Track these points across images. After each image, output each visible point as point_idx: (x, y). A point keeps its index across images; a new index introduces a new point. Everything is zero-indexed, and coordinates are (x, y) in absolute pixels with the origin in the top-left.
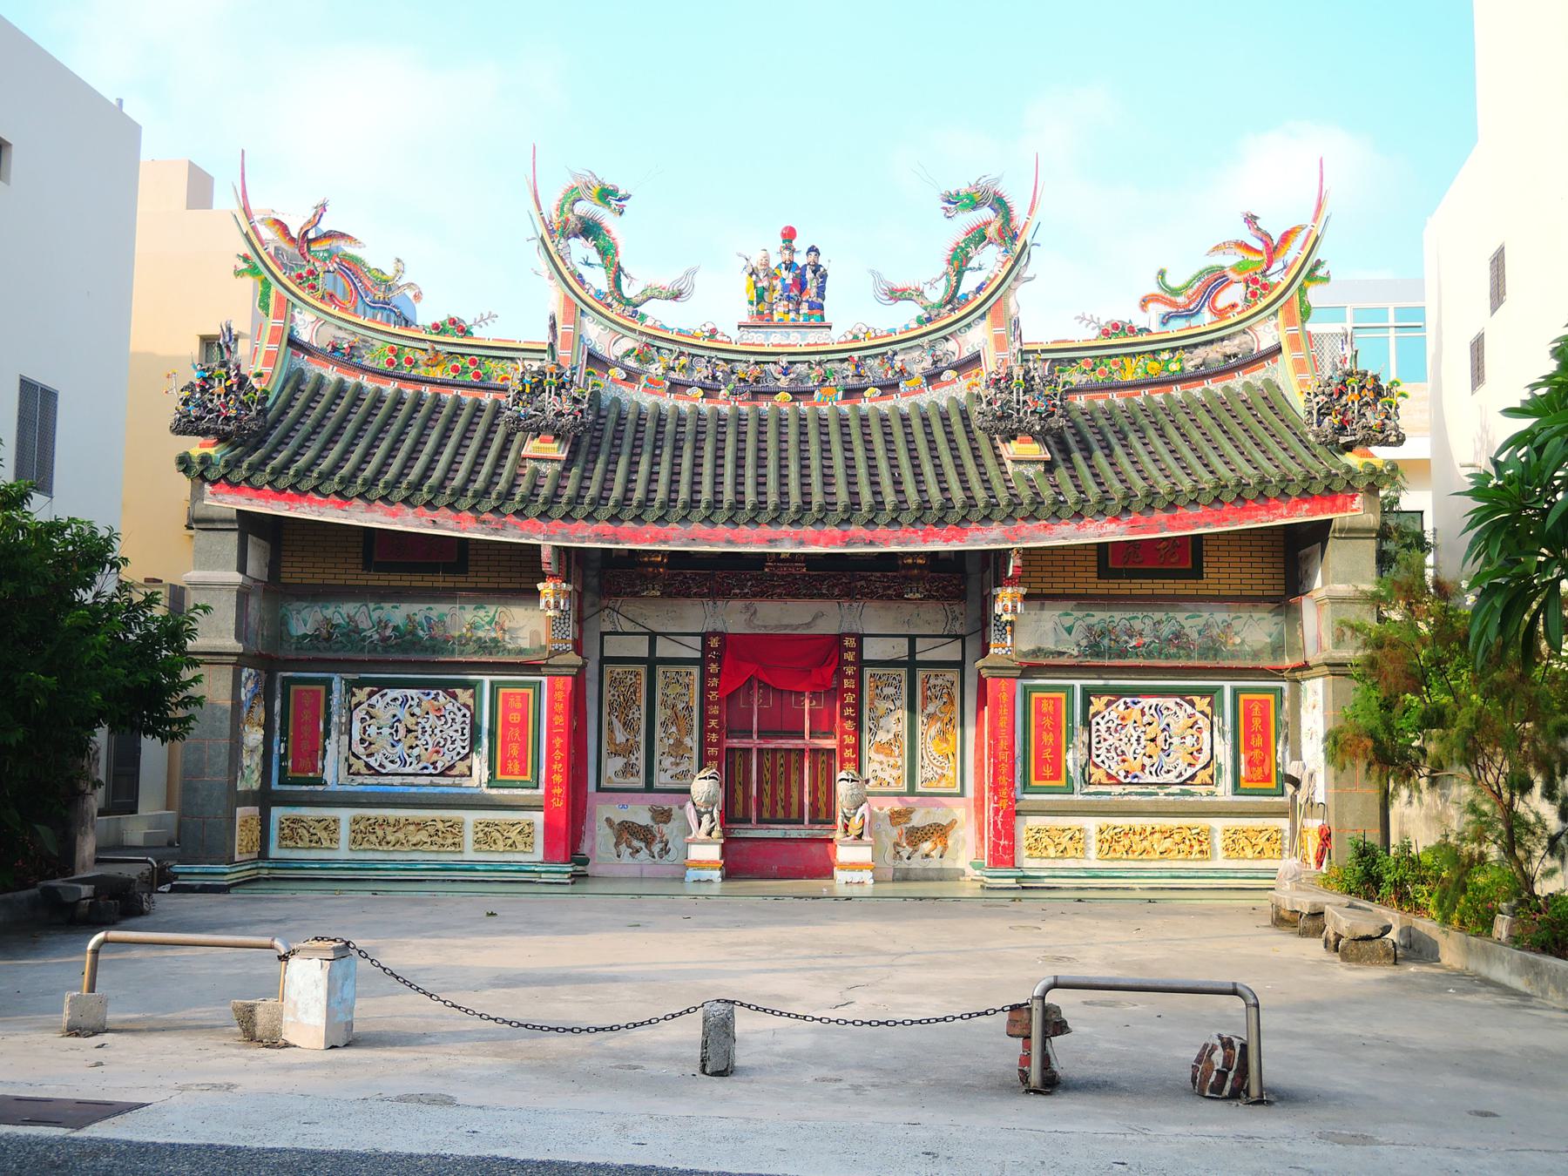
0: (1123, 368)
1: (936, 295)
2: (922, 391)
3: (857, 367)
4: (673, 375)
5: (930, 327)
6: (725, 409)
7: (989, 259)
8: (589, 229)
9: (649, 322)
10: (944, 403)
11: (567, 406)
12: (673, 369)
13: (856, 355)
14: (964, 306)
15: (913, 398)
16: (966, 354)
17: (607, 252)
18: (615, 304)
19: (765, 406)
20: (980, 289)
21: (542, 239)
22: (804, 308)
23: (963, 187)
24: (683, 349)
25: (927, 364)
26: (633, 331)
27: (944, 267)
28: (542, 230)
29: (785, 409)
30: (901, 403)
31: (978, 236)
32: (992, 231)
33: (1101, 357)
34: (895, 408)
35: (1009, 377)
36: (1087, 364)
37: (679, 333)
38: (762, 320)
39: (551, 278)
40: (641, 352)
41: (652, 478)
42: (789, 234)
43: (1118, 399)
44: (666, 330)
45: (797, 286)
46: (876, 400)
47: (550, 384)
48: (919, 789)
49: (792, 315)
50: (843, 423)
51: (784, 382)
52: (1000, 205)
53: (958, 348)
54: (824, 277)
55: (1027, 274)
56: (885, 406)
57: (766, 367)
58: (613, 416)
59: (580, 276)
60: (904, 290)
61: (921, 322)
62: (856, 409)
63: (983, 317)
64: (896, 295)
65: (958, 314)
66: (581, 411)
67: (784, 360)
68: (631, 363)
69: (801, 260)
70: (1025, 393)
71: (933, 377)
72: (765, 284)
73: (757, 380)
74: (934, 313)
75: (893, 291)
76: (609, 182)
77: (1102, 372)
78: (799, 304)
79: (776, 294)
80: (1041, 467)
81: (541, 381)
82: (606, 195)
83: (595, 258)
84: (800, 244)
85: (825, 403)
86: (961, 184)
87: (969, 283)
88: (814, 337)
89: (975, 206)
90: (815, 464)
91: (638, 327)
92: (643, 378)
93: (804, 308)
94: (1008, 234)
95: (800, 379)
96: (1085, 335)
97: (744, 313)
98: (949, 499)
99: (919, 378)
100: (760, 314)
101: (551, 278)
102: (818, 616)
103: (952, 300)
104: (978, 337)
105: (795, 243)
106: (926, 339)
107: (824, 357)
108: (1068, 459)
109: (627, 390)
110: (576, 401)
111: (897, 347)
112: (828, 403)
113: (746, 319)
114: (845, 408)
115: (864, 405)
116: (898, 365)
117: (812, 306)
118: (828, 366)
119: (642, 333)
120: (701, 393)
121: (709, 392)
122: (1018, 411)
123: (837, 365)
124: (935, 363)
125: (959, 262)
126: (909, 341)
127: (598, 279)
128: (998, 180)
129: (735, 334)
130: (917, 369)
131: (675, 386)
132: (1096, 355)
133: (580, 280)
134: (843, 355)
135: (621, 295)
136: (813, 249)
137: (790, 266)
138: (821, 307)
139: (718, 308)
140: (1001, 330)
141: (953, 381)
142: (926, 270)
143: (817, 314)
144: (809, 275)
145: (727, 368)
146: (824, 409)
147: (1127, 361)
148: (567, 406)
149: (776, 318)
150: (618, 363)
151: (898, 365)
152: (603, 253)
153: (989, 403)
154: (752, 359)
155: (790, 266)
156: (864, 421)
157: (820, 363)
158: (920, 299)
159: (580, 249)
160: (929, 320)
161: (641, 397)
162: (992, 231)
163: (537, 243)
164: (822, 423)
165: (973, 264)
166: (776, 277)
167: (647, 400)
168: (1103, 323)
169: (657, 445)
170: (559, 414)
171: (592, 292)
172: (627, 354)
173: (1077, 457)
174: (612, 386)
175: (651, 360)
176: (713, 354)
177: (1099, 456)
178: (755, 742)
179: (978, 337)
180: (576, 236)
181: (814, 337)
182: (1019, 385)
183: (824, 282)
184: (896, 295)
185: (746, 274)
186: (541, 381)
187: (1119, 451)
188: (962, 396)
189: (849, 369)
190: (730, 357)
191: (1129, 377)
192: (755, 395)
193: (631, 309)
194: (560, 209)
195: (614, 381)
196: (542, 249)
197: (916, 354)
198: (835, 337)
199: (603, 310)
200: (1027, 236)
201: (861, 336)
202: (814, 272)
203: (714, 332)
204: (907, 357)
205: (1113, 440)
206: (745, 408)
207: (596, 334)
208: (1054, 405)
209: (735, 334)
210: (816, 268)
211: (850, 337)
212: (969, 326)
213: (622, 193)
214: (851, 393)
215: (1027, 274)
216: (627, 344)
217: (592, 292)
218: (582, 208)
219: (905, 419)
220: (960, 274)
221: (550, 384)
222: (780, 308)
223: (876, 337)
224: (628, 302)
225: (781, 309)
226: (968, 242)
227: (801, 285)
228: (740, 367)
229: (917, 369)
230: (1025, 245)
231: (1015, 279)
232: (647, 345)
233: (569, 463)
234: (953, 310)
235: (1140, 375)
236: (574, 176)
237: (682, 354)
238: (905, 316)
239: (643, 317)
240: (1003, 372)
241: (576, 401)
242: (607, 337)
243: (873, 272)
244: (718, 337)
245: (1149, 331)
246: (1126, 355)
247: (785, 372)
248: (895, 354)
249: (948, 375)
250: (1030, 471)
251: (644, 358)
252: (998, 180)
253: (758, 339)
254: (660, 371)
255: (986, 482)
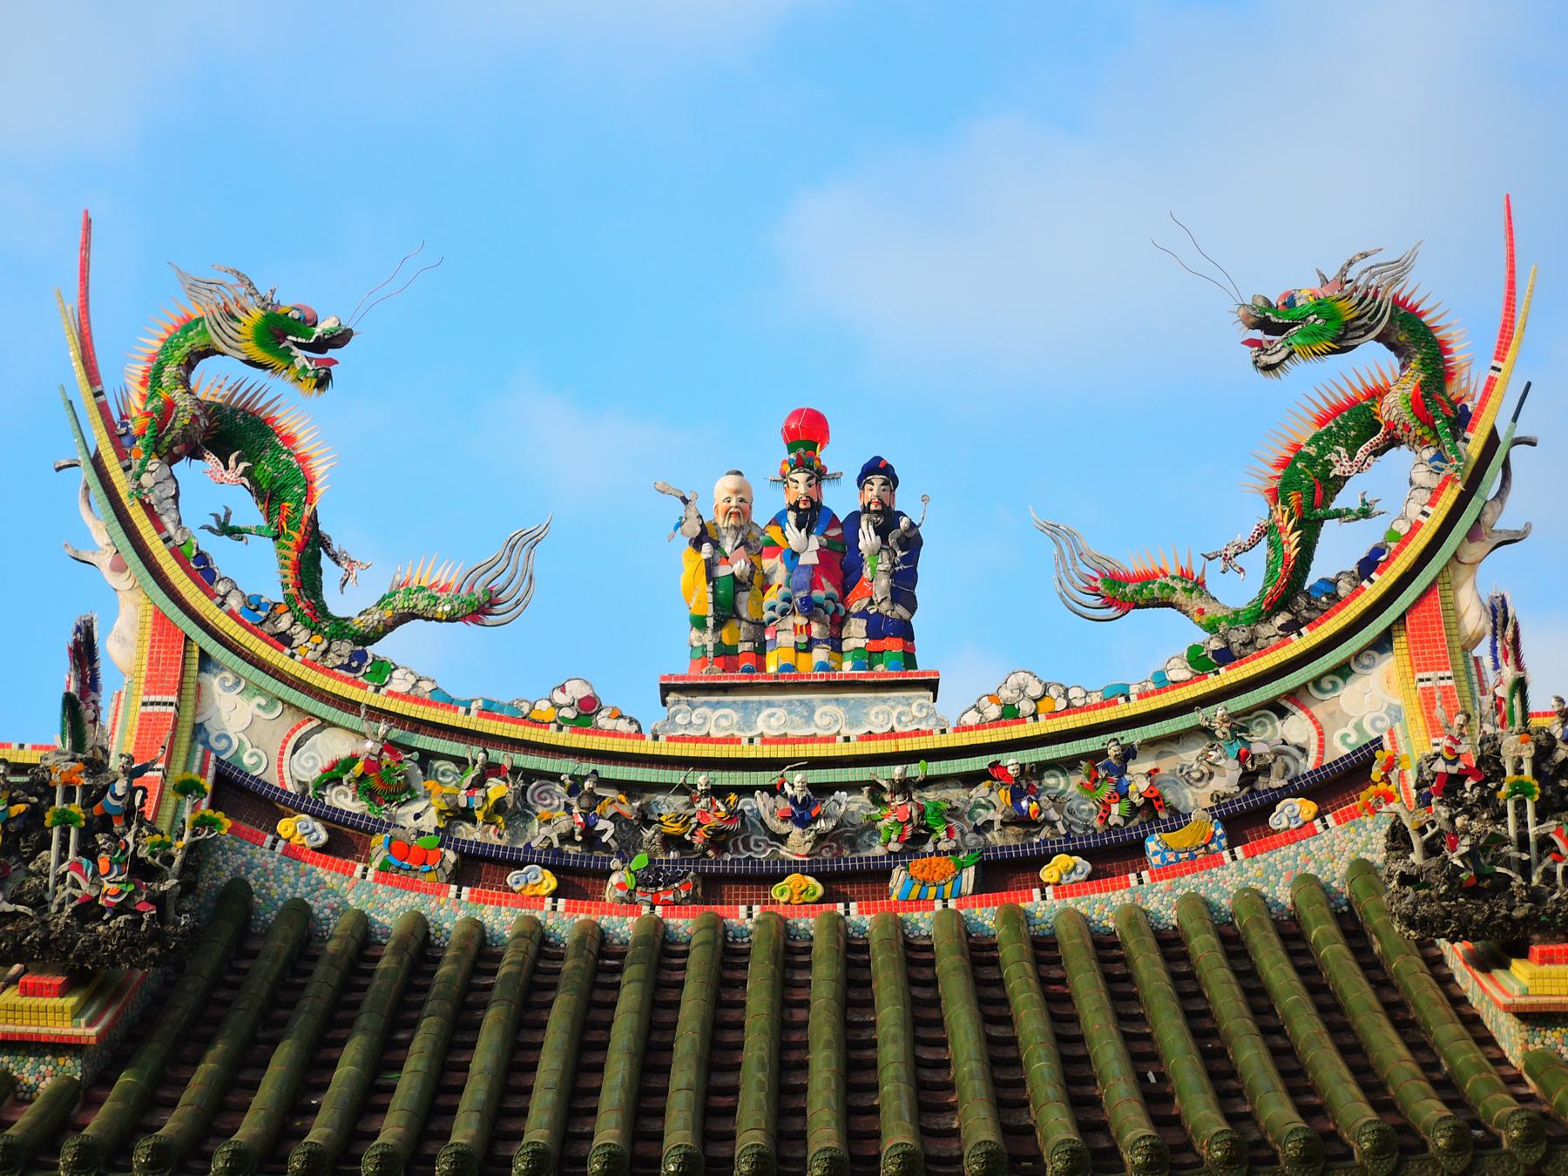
1: (1243, 587)
2: (1214, 860)
3: (1017, 795)
4: (469, 833)
5: (1229, 676)
6: (623, 927)
7: (1395, 491)
8: (232, 433)
9: (400, 683)
10: (1283, 895)
11: (112, 887)
12: (467, 815)
13: (1011, 761)
14: (1326, 614)
15: (1190, 883)
16: (1339, 749)
17: (281, 494)
18: (301, 635)
19: (743, 917)
20: (1369, 565)
21: (97, 462)
22: (856, 635)
23: (1306, 288)
24: (498, 755)
25: (1226, 780)
26: (350, 706)
27: (1258, 511)
28: (99, 439)
29: (805, 923)
30: (1156, 895)
31: (1358, 425)
32: (1395, 407)
34: (1136, 916)
35: (1490, 765)
37: (488, 711)
38: (733, 672)
39: (119, 567)
40: (372, 766)
41: (370, 1098)
42: (807, 434)
44: (450, 704)
45: (836, 571)
46: (1075, 889)
47: (65, 821)
48: (1078, 703)
49: (820, 654)
50: (980, 954)
51: (798, 844)
52: (1410, 333)
54: (912, 543)
55: (1506, 521)
56: (1105, 906)
57: (746, 804)
58: (279, 945)
59: (202, 558)
60: (1147, 578)
61: (1200, 663)
62: (1018, 919)
63: (1383, 643)
64: (1123, 593)
66: (159, 900)
67: (796, 782)
68: (344, 800)
69: (842, 499)
70: (1541, 817)
71: (1244, 821)
72: (739, 566)
73: (719, 840)
74: (1238, 637)
75: (1116, 580)
76: (289, 300)
78: (838, 622)
79: (773, 597)
81: (36, 814)
82: (281, 334)
83: (248, 512)
84: (842, 456)
85: (921, 902)
86: (1298, 276)
87: (1337, 551)
88: (888, 718)
89: (1342, 342)
90: (891, 1054)
91: (367, 696)
92: (379, 842)
93: (856, 635)
94: (1441, 412)
95: (848, 834)
97: (682, 649)
98: (1333, 1136)
99: (1203, 826)
100: (725, 653)
101: (119, 567)
102: (123, 641)
103: (1291, 596)
104: (1379, 705)
105: (827, 456)
106: (1219, 710)
107: (917, 770)
109: (326, 875)
110: (140, 870)
111: (1134, 736)
112: (933, 903)
113: (681, 667)
114: (986, 916)
115: (1042, 906)
116: (1139, 785)
117: (877, 627)
118: (931, 795)
119: (376, 714)
120: (550, 882)
121: (577, 878)
122: (1525, 869)
123: (956, 795)
124: (1247, 779)
125: (1308, 492)
126: (1170, 723)
127: (257, 568)
128: (1401, 267)
129: (652, 714)
130: (1196, 799)
131: (476, 868)
133: (202, 569)
134: (973, 763)
135: (326, 615)
136: (876, 468)
137: (810, 515)
138: (905, 631)
139: (605, 648)
140: (1438, 678)
142: (1219, 524)
143: (893, 646)
144: (867, 539)
145: (629, 809)
146: (922, 921)
148: (112, 887)
149: (771, 668)
150: (307, 802)
151: (1139, 785)
152: (268, 496)
153: (1431, 849)
154: (701, 779)
155: (810, 515)
156: (1044, 949)
157: (904, 787)
158: (1195, 602)
159: (210, 488)
160: (1225, 657)
161: (371, 896)
162: (1395, 407)
163: (86, 473)
164: (916, 957)
165: (1346, 499)
166: (773, 547)
167: (390, 908)
169: (401, 1018)
170: (88, 911)
171: (234, 602)
172: (332, 776)
174: (286, 866)
175: (403, 792)
176: (586, 768)
179: (1379, 705)
180: (195, 454)
181: (888, 718)
182: (1521, 789)
183: (912, 559)
184: (1123, 593)
185: (683, 542)
186: (36, 814)
188: (1336, 873)
189: (993, 802)
190: (638, 779)
192: (713, 887)
193: (346, 647)
194: (153, 379)
195: (293, 853)
196: (97, 489)
197: (1190, 756)
198: (955, 711)
199: (264, 650)
200: (1496, 416)
201: (1026, 707)
202: (882, 531)
203: (588, 708)
204: (1167, 765)
206: (683, 924)
207: (241, 719)
209: (652, 714)
210: (887, 520)
211: (993, 712)
212: (1343, 671)
213: (325, 325)
214: (1003, 872)
215: (1506, 521)
216: (333, 746)
217: (234, 602)
218: (217, 380)
219: (1170, 944)
220: (1309, 528)
221: (65, 821)
222: (785, 638)
223: (1070, 708)
224: (341, 629)
225: (787, 639)
226: (1325, 440)
227: (841, 563)
228: (669, 807)
229: (1196, 799)
230: (1493, 441)
231: (1473, 535)
232: (391, 746)
233: (106, 1062)
234: (1293, 627)
236: (194, 287)
237: (492, 769)
238: (1150, 655)
239: (383, 670)
240: (1469, 750)
241: (140, 870)
242: (276, 726)
243: (1053, 530)
244: (603, 720)
247: (802, 814)
248: (1129, 753)
249: (1291, 812)
251: (382, 785)
252: (1401, 267)
253: (719, 724)
254: (430, 821)
255: (1447, 1087)
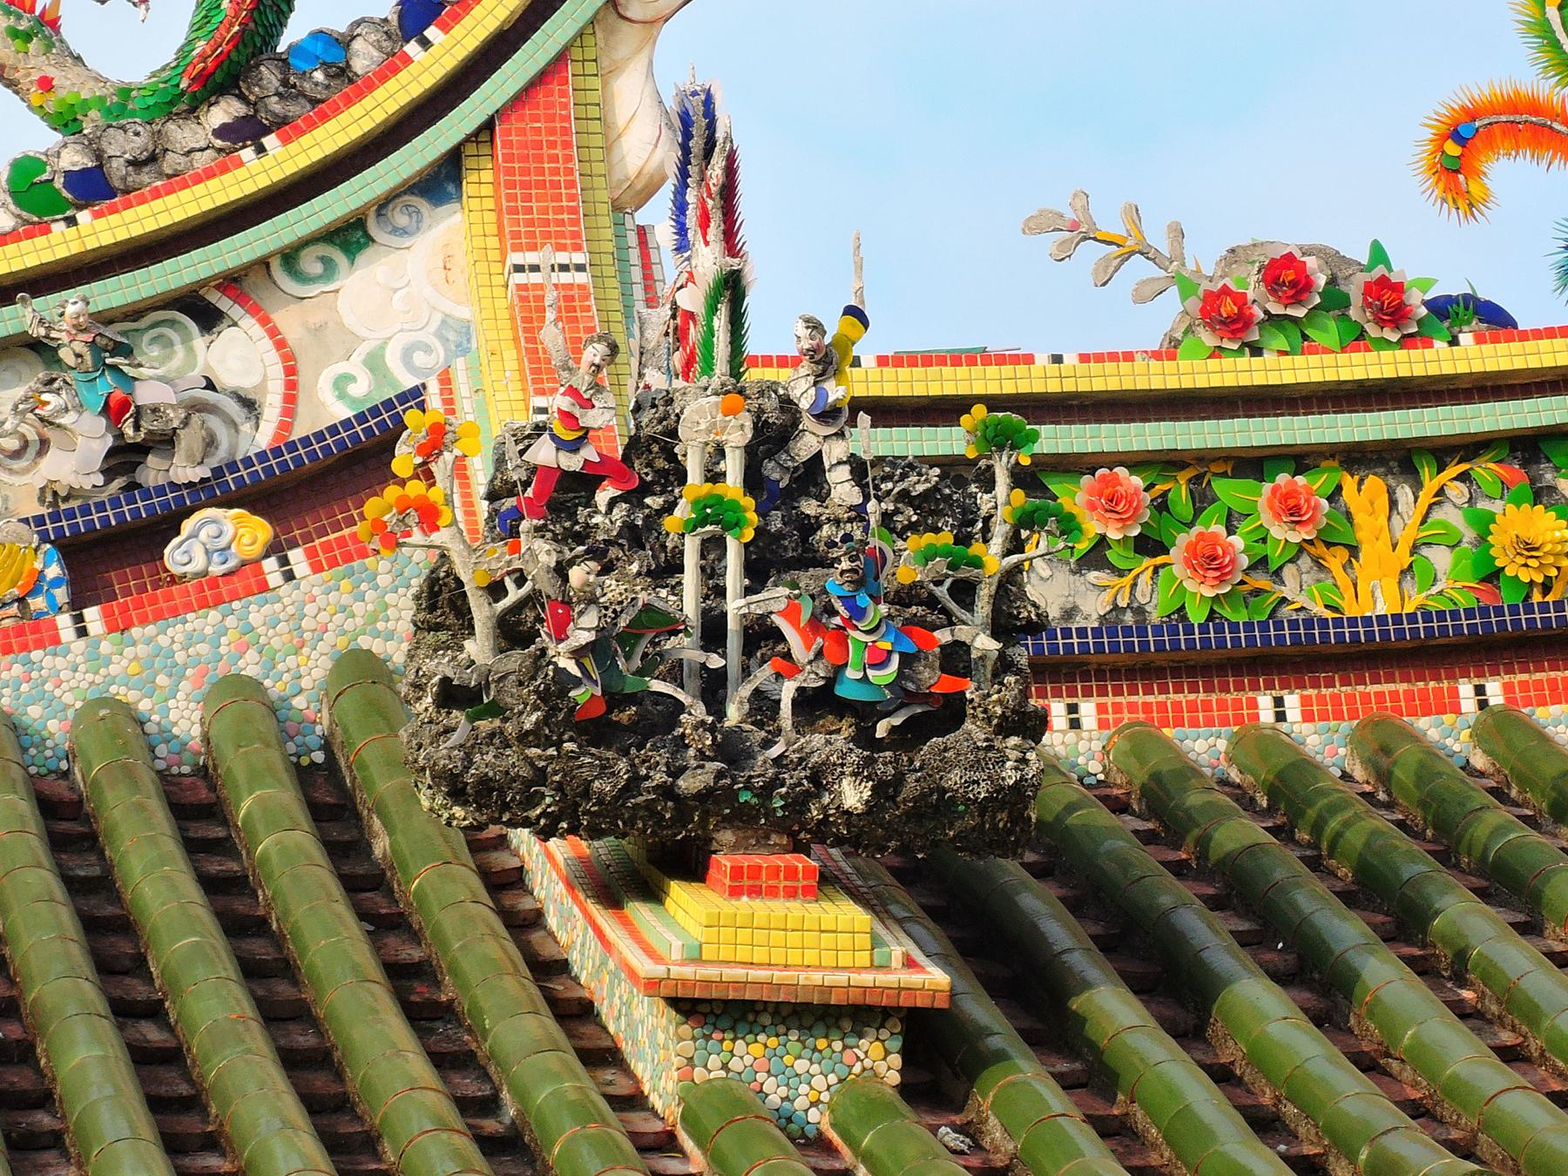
0: (1335, 540)
5: (98, 230)
10: (183, 718)
14: (321, 109)
16: (329, 405)
33: (1200, 467)
35: (653, 458)
36: (1112, 503)
43: (1312, 728)
53: (259, 376)
63: (442, 180)
65: (280, 160)
70: (757, 574)
74: (123, 146)
77: (1209, 561)
80: (879, 1059)
96: (1118, 330)
104: (418, 318)
108: (1053, 1027)
122: (713, 688)
124: (123, 459)
132: (1181, 454)
141: (243, 580)
147: (1365, 495)
153: (512, 633)
158: (35, 62)
160: (92, 188)
168: (1204, 256)
173: (1113, 1009)
177: (1260, 1006)
178: (1197, 636)
179: (418, 318)
182: (715, 514)
187: (1384, 975)
188: (303, 680)
191: (1377, 594)
205: (1346, 930)
208: (956, 658)
212: (349, 236)
234: (246, 132)
235: (1448, 583)
240: (610, 422)
245: (1495, 320)
246: (1356, 457)
249: (213, 538)
250: (805, 1080)
